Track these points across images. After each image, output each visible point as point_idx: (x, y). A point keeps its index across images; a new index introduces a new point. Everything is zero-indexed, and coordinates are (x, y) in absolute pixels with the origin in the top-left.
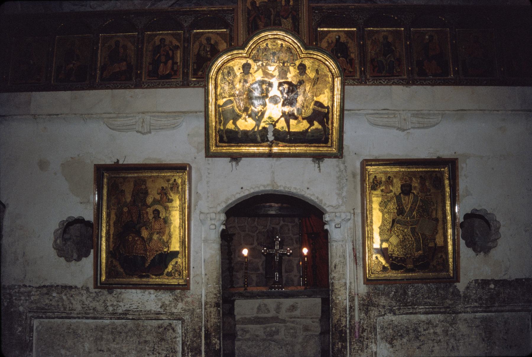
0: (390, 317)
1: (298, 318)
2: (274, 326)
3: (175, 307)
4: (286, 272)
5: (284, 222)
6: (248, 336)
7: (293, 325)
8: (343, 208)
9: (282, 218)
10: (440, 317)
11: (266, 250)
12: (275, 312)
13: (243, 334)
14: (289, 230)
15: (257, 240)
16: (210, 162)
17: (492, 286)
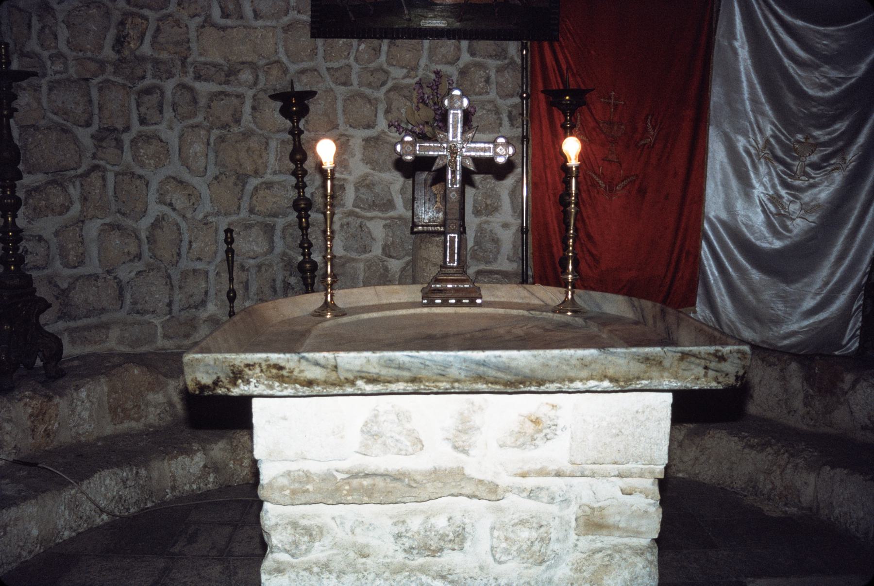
1: (558, 474)
2: (443, 512)
4: (477, 213)
5: (473, 54)
6: (319, 552)
7: (532, 505)
9: (464, 44)
11: (413, 144)
12: (448, 448)
13: (296, 544)
14: (487, 81)
15: (387, 111)
16: (728, 481)
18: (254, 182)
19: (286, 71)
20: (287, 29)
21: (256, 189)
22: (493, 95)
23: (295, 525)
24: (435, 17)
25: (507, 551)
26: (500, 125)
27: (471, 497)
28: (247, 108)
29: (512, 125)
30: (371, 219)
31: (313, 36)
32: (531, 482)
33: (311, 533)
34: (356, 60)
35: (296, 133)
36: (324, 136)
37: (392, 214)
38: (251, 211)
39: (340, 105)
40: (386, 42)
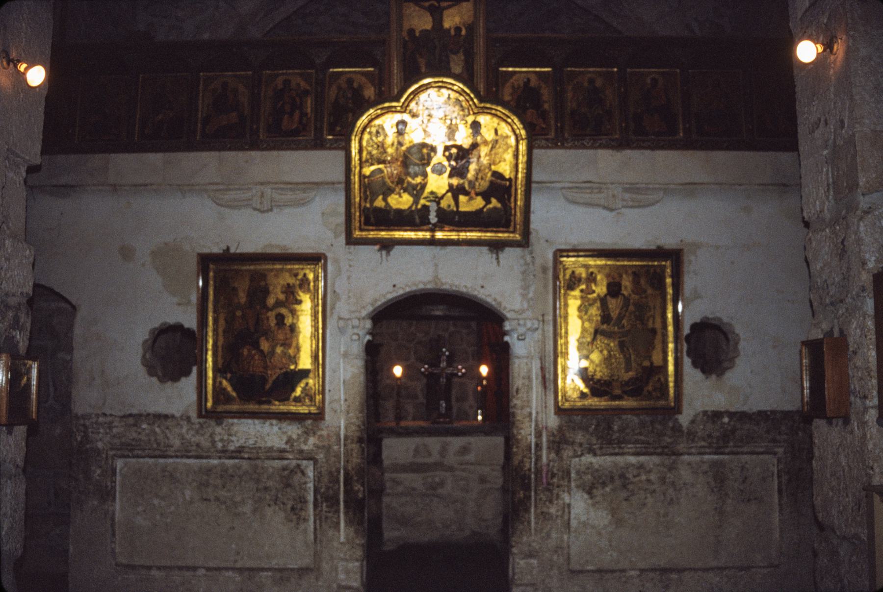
0: (588, 459)
3: (305, 442)
6: (400, 489)
8: (529, 314)
10: (656, 459)
17: (726, 420)
32: (463, 467)
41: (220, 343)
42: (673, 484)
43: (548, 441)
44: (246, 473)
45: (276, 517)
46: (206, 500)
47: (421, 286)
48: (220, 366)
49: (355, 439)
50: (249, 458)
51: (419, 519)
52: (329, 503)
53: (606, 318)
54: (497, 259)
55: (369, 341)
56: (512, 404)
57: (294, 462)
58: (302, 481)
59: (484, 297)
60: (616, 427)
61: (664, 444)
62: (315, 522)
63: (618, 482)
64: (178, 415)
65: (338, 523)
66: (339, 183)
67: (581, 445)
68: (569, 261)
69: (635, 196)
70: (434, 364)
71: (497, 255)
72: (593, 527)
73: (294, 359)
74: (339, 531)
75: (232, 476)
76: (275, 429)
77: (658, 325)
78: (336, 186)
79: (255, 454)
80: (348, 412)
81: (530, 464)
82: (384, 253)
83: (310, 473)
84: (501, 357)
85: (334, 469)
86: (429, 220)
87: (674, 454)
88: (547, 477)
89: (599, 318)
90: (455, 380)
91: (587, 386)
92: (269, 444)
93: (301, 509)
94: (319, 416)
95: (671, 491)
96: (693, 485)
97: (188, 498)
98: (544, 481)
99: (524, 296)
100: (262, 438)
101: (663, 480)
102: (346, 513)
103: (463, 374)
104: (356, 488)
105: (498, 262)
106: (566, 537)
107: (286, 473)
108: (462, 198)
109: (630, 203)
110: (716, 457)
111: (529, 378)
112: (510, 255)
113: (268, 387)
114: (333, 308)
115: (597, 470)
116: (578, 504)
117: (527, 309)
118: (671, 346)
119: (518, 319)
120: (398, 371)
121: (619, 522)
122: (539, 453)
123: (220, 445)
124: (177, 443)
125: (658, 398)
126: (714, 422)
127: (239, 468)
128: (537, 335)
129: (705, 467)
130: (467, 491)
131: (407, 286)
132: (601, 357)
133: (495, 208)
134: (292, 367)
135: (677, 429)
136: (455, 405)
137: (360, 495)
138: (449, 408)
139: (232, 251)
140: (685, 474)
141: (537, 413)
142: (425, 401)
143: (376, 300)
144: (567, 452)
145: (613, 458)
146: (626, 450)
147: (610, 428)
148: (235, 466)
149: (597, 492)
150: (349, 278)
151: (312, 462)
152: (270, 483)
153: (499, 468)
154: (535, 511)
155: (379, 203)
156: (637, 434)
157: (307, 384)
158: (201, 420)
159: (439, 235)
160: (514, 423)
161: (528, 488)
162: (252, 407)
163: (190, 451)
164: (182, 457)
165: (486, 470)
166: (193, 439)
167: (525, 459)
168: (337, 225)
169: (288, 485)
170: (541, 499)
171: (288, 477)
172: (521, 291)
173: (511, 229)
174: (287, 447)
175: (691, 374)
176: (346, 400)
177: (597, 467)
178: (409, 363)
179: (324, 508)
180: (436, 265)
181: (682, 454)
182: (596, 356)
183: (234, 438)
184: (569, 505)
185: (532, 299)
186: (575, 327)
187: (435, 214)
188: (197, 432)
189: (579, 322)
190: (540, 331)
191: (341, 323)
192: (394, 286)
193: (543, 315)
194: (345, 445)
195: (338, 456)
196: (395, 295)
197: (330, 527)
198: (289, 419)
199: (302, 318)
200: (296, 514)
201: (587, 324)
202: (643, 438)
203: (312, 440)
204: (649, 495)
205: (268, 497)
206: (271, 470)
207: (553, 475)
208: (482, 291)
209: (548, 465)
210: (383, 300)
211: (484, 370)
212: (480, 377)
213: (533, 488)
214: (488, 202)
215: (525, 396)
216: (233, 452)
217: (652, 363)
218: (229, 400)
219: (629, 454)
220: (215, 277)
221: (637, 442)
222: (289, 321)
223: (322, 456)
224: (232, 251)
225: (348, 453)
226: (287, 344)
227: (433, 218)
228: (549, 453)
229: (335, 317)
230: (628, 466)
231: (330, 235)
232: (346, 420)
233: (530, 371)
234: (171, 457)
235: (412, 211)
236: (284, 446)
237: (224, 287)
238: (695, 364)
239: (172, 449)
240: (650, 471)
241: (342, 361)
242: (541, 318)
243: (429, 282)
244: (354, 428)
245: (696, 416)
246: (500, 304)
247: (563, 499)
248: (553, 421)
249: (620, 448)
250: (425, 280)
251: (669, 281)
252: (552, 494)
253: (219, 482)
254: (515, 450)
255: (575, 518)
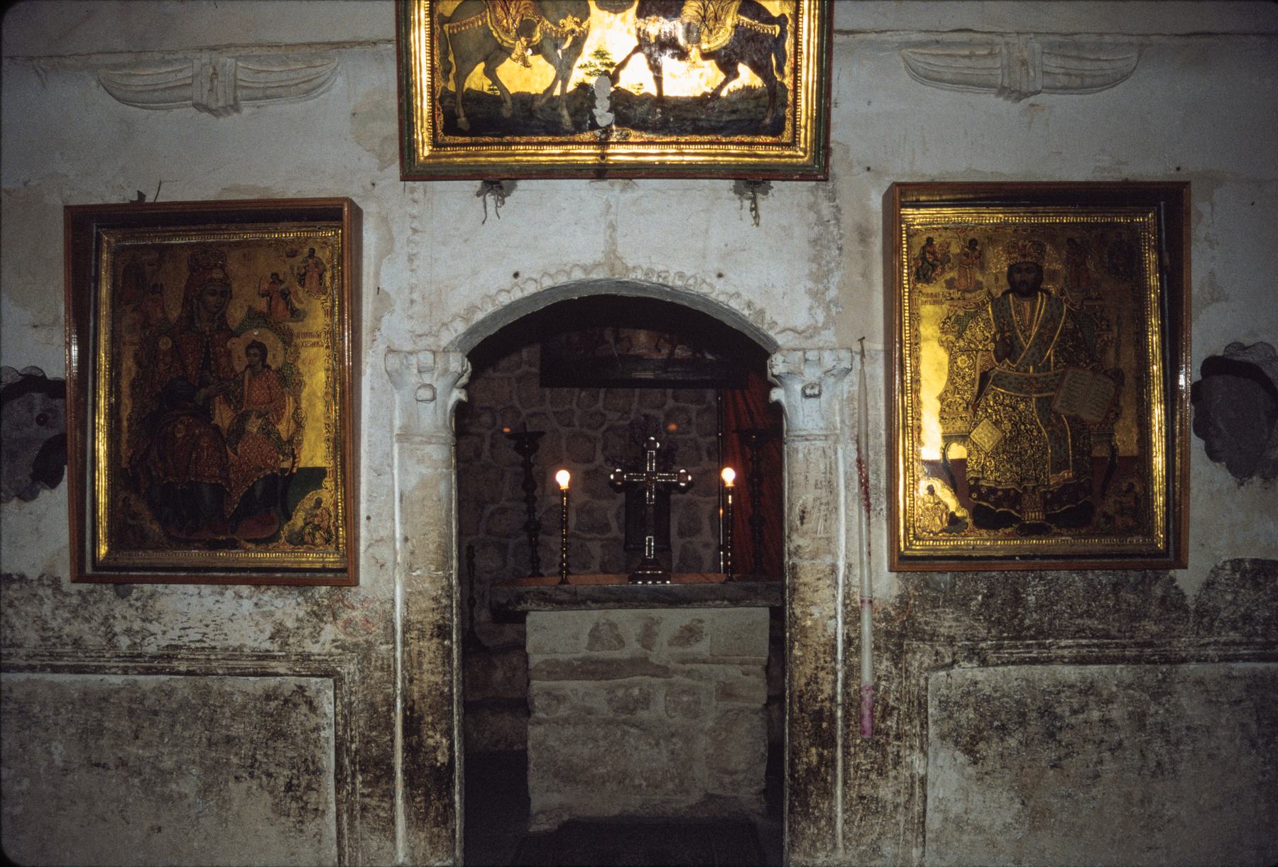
0: (968, 671)
2: (637, 684)
6: (563, 711)
7: (688, 681)
8: (828, 336)
9: (670, 392)
11: (622, 474)
13: (549, 705)
15: (604, 449)
18: (492, 507)
19: (518, 414)
20: (519, 380)
21: (492, 514)
22: (694, 434)
23: (549, 694)
24: (645, 370)
25: (675, 710)
26: (701, 459)
27: (652, 676)
28: (487, 446)
29: (710, 459)
30: (590, 540)
31: (543, 384)
32: (688, 667)
33: (560, 699)
34: (578, 405)
35: (527, 466)
36: (735, 469)
37: (610, 535)
38: (488, 532)
39: (563, 442)
40: (603, 390)
41: (125, 413)
42: (1163, 730)
43: (876, 632)
44: (184, 705)
45: (252, 804)
46: (98, 765)
47: (578, 275)
48: (124, 465)
49: (428, 629)
50: (189, 673)
51: (602, 770)
52: (370, 777)
53: (1006, 348)
54: (754, 209)
55: (459, 406)
56: (789, 546)
57: (292, 682)
58: (311, 724)
59: (721, 298)
60: (1032, 598)
61: (1141, 637)
62: (339, 816)
63: (1035, 726)
64: (32, 574)
65: (392, 821)
66: (389, 41)
67: (951, 640)
68: (916, 217)
69: (1073, 64)
70: (637, 465)
71: (754, 200)
72: (979, 829)
73: (291, 446)
74: (394, 839)
75: (156, 713)
76: (247, 605)
77: (1127, 360)
78: (381, 47)
79: (207, 662)
80: (411, 568)
81: (832, 686)
82: (490, 199)
83: (328, 706)
84: (761, 437)
85: (379, 698)
86: (593, 118)
87: (1167, 660)
88: (872, 716)
89: (991, 346)
90: (674, 497)
91: (963, 504)
92: (233, 642)
93: (309, 788)
94: (345, 575)
95: (1158, 745)
96: (1208, 731)
97: (58, 762)
98: (867, 723)
99: (815, 295)
100: (218, 627)
101: (1139, 719)
102: (409, 799)
103: (690, 485)
104: (431, 742)
105: (757, 217)
106: (916, 853)
107: (273, 704)
108: (667, 61)
109: (1063, 80)
110: (1261, 666)
111: (831, 487)
112: (784, 199)
113: (230, 509)
114: (376, 328)
115: (988, 699)
116: (943, 774)
117: (825, 327)
118: (1158, 412)
119: (804, 351)
120: (563, 478)
121: (1037, 817)
122: (855, 660)
123: (124, 642)
124: (31, 637)
125: (1130, 531)
126: (1257, 586)
127: (169, 694)
128: (849, 386)
129: (1236, 691)
130: (696, 716)
131: (545, 274)
132: (997, 435)
133: (749, 90)
134: (286, 465)
135: (1173, 603)
136: (676, 541)
137: (442, 758)
138: (664, 545)
139: (149, 199)
140: (1190, 705)
141: (849, 566)
142: (622, 536)
143: (473, 309)
144: (920, 658)
145: (1024, 670)
146: (1054, 652)
147: (1017, 599)
148: (159, 689)
149: (990, 750)
150: (411, 258)
151: (330, 681)
152: (237, 729)
153: (759, 668)
154: (844, 796)
155: (477, 80)
156: (1081, 616)
157: (319, 502)
158: (84, 587)
159: (620, 154)
160: (794, 590)
161: (826, 740)
162: (196, 556)
163: (61, 656)
164: (43, 669)
165: (734, 671)
166: (67, 629)
167: (821, 674)
168: (386, 138)
169: (279, 734)
170: (857, 767)
171: (278, 714)
172: (810, 285)
173: (786, 136)
174: (274, 647)
175: (1207, 476)
176: (406, 539)
177: (988, 691)
178: (590, 467)
179: (359, 786)
180: (612, 227)
181: (1184, 661)
182: (985, 435)
183: (155, 627)
184: (923, 781)
185: (834, 301)
186: (933, 367)
187: (607, 104)
188: (75, 612)
189: (943, 356)
190: (854, 377)
191: (394, 362)
192: (516, 275)
193: (861, 340)
194: (405, 643)
195: (389, 669)
196: (517, 295)
197: (373, 830)
198: (277, 583)
199: (308, 353)
200: (296, 799)
201: (962, 361)
202: (1094, 623)
203: (330, 631)
204: (1107, 755)
205: (234, 760)
206: (239, 699)
207: (887, 712)
208: (720, 285)
209: (875, 688)
210: (490, 309)
211: (729, 475)
212: (722, 489)
213: (840, 742)
214: (731, 73)
215: (820, 527)
216: (154, 658)
217: (1114, 450)
218: (142, 541)
219: (1061, 660)
220: (114, 266)
221: (1079, 633)
222: (276, 358)
223: (352, 668)
224: (149, 199)
225: (412, 662)
226: (273, 409)
227: (603, 115)
228: (877, 659)
229: (382, 348)
230: (1062, 686)
231: (369, 162)
232: (408, 584)
233: (831, 470)
234: (19, 669)
235: (553, 99)
236: (267, 645)
237: (135, 285)
238: (1213, 454)
239: (22, 652)
240: (1109, 701)
241: (396, 447)
242: (857, 347)
243: (597, 265)
244: (427, 604)
245: (1216, 571)
246: (761, 312)
247: (910, 766)
248: (886, 585)
249: (1040, 646)
250: (588, 260)
251: (1151, 258)
252: (884, 756)
253: (125, 725)
254: (797, 652)
255: (937, 809)
